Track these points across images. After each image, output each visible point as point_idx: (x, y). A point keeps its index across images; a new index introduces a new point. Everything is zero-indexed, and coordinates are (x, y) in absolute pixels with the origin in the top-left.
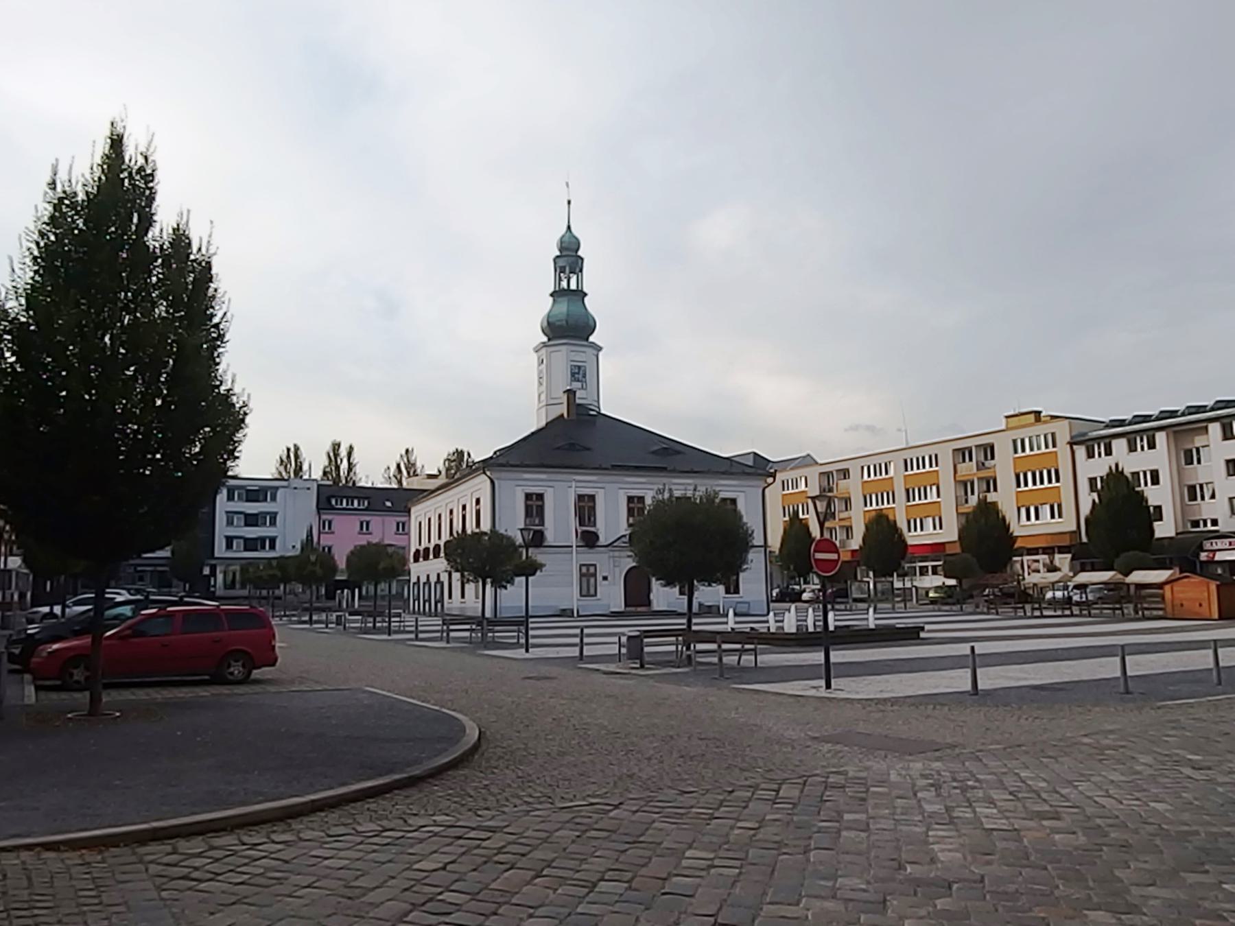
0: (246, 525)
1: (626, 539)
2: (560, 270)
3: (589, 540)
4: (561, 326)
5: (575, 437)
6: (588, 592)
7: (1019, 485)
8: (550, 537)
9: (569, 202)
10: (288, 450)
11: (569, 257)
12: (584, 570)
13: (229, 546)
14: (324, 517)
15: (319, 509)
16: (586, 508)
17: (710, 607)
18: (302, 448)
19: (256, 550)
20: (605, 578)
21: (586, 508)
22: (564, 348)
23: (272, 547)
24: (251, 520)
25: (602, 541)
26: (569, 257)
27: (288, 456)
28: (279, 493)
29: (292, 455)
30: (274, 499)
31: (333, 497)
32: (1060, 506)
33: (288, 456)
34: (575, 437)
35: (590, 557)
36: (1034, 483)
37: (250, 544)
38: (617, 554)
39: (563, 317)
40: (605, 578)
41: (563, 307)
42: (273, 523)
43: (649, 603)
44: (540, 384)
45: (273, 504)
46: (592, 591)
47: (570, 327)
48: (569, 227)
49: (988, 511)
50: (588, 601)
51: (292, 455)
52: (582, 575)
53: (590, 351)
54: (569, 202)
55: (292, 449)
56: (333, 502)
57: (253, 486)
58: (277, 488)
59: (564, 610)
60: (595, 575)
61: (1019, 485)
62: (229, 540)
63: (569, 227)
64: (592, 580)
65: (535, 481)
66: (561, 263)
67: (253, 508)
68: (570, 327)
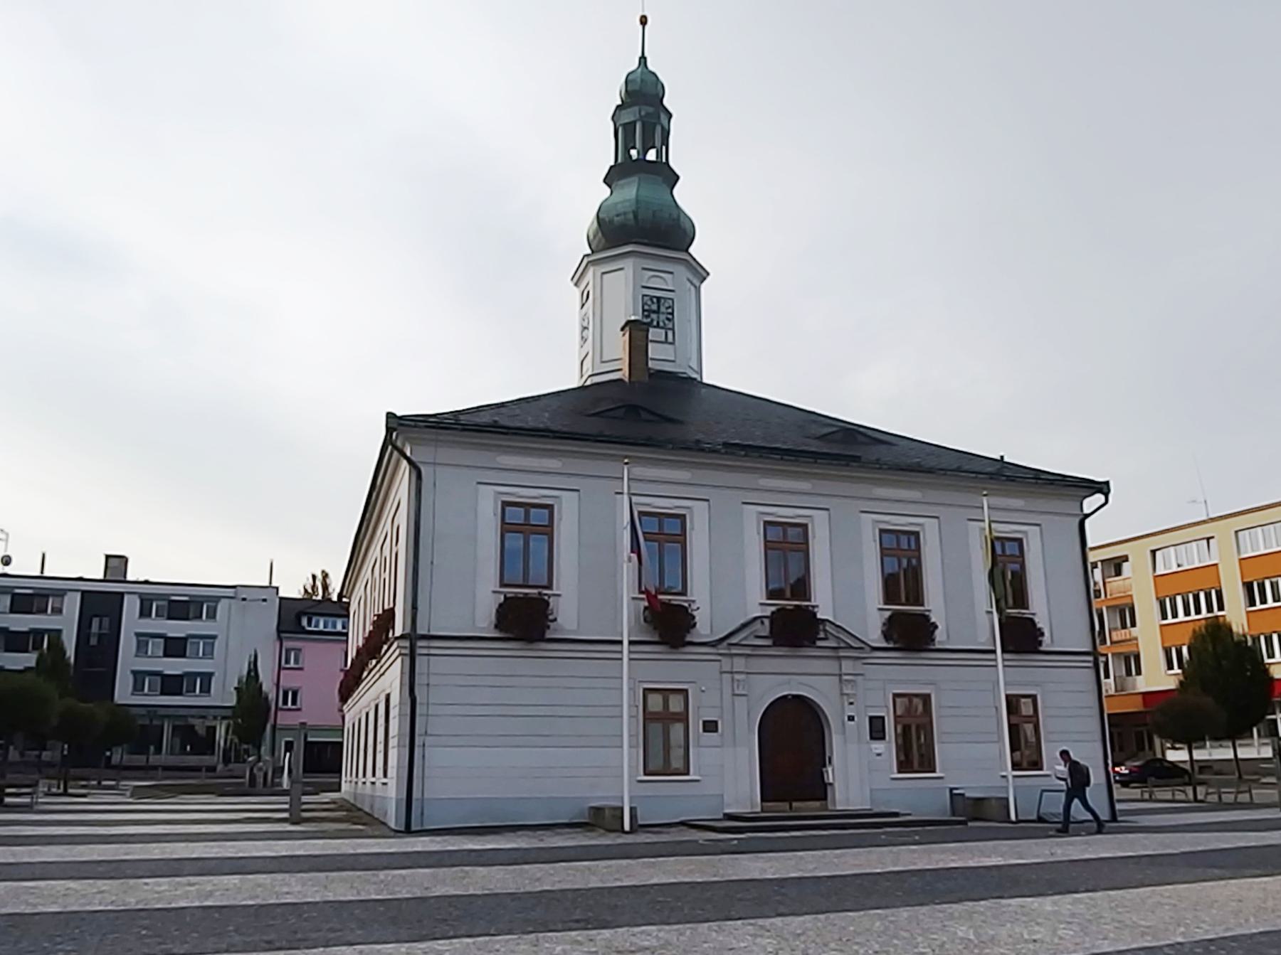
0: (166, 655)
1: (765, 629)
2: (624, 133)
3: (668, 623)
4: (623, 226)
5: (644, 409)
6: (663, 759)
7: (1164, 617)
8: (568, 613)
9: (644, 21)
10: (314, 577)
11: (643, 111)
12: (656, 703)
13: (138, 688)
14: (287, 644)
15: (279, 631)
16: (661, 537)
17: (979, 801)
18: (331, 575)
19: (180, 694)
20: (710, 726)
21: (661, 537)
22: (628, 264)
23: (206, 690)
24: (175, 647)
25: (704, 628)
26: (643, 111)
27: (314, 586)
28: (222, 607)
29: (319, 584)
30: (212, 615)
31: (305, 614)
32: (1137, 658)
33: (314, 586)
34: (644, 409)
35: (669, 670)
36: (1187, 613)
37: (171, 684)
38: (739, 664)
39: (629, 208)
40: (710, 726)
41: (629, 191)
42: (209, 654)
43: (820, 790)
44: (584, 339)
45: (210, 623)
46: (677, 763)
47: (644, 226)
48: (643, 59)
49: (1217, 631)
50: (666, 788)
51: (319, 584)
52: (649, 717)
53: (680, 270)
54: (644, 21)
55: (320, 577)
56: (304, 622)
57: (180, 595)
58: (217, 599)
59: (597, 811)
60: (683, 718)
61: (1164, 617)
62: (139, 676)
63: (643, 59)
64: (677, 730)
65: (532, 475)
66: (627, 117)
67: (177, 628)
68: (644, 226)
